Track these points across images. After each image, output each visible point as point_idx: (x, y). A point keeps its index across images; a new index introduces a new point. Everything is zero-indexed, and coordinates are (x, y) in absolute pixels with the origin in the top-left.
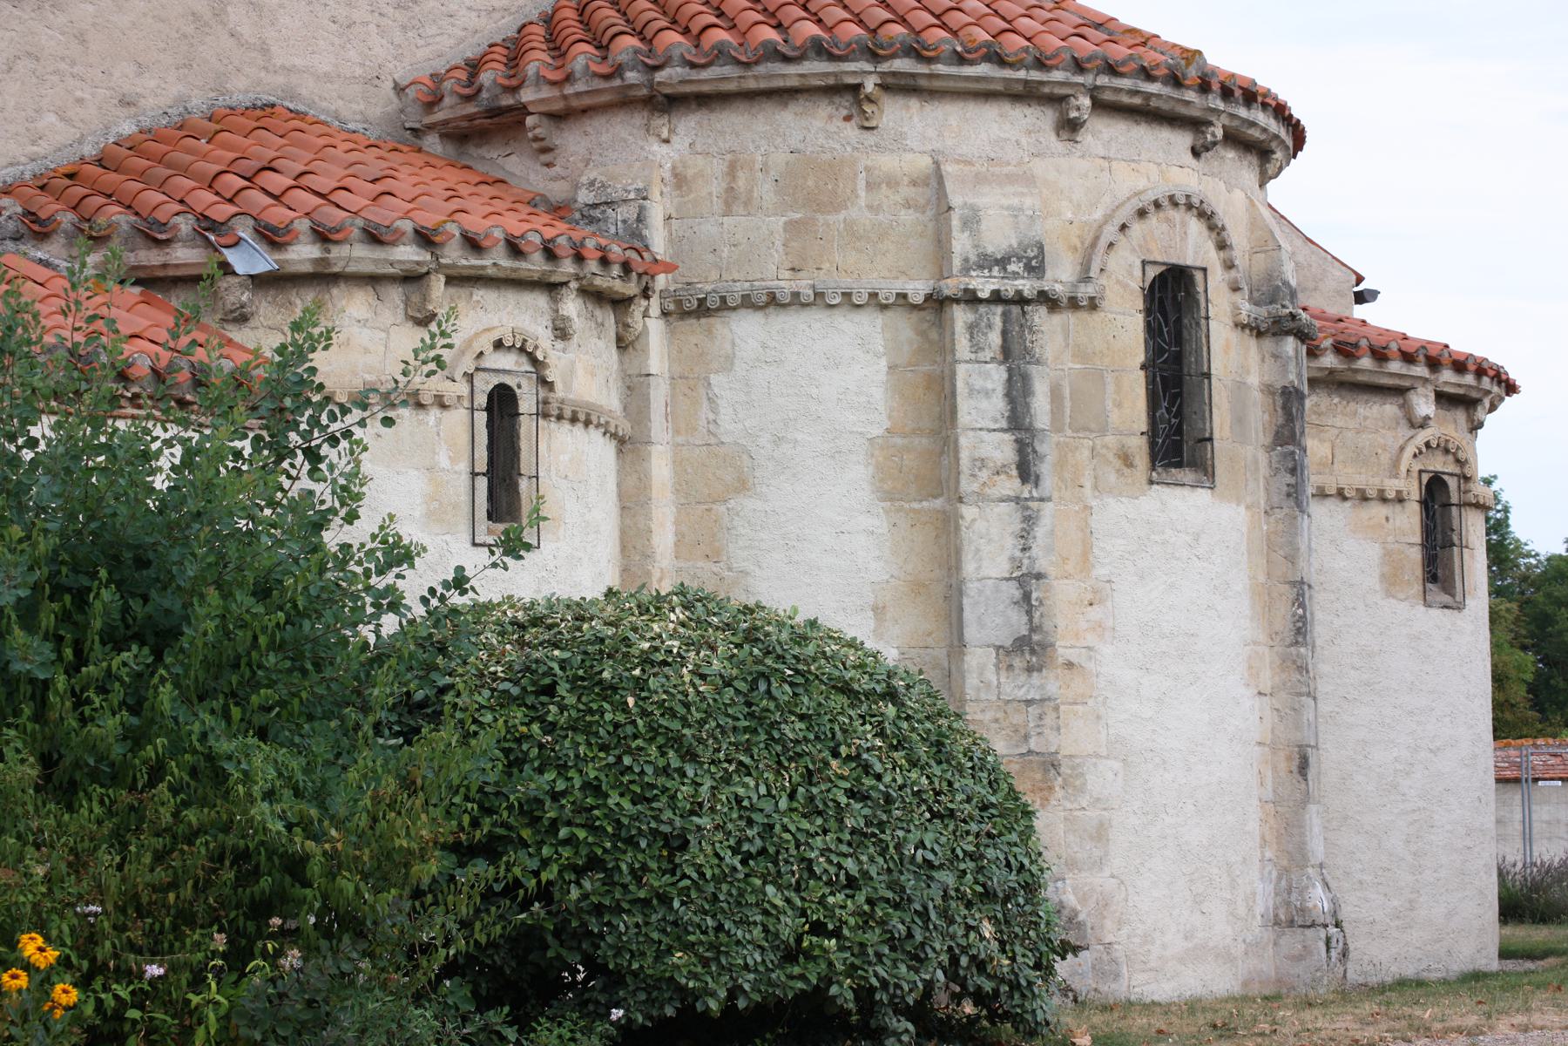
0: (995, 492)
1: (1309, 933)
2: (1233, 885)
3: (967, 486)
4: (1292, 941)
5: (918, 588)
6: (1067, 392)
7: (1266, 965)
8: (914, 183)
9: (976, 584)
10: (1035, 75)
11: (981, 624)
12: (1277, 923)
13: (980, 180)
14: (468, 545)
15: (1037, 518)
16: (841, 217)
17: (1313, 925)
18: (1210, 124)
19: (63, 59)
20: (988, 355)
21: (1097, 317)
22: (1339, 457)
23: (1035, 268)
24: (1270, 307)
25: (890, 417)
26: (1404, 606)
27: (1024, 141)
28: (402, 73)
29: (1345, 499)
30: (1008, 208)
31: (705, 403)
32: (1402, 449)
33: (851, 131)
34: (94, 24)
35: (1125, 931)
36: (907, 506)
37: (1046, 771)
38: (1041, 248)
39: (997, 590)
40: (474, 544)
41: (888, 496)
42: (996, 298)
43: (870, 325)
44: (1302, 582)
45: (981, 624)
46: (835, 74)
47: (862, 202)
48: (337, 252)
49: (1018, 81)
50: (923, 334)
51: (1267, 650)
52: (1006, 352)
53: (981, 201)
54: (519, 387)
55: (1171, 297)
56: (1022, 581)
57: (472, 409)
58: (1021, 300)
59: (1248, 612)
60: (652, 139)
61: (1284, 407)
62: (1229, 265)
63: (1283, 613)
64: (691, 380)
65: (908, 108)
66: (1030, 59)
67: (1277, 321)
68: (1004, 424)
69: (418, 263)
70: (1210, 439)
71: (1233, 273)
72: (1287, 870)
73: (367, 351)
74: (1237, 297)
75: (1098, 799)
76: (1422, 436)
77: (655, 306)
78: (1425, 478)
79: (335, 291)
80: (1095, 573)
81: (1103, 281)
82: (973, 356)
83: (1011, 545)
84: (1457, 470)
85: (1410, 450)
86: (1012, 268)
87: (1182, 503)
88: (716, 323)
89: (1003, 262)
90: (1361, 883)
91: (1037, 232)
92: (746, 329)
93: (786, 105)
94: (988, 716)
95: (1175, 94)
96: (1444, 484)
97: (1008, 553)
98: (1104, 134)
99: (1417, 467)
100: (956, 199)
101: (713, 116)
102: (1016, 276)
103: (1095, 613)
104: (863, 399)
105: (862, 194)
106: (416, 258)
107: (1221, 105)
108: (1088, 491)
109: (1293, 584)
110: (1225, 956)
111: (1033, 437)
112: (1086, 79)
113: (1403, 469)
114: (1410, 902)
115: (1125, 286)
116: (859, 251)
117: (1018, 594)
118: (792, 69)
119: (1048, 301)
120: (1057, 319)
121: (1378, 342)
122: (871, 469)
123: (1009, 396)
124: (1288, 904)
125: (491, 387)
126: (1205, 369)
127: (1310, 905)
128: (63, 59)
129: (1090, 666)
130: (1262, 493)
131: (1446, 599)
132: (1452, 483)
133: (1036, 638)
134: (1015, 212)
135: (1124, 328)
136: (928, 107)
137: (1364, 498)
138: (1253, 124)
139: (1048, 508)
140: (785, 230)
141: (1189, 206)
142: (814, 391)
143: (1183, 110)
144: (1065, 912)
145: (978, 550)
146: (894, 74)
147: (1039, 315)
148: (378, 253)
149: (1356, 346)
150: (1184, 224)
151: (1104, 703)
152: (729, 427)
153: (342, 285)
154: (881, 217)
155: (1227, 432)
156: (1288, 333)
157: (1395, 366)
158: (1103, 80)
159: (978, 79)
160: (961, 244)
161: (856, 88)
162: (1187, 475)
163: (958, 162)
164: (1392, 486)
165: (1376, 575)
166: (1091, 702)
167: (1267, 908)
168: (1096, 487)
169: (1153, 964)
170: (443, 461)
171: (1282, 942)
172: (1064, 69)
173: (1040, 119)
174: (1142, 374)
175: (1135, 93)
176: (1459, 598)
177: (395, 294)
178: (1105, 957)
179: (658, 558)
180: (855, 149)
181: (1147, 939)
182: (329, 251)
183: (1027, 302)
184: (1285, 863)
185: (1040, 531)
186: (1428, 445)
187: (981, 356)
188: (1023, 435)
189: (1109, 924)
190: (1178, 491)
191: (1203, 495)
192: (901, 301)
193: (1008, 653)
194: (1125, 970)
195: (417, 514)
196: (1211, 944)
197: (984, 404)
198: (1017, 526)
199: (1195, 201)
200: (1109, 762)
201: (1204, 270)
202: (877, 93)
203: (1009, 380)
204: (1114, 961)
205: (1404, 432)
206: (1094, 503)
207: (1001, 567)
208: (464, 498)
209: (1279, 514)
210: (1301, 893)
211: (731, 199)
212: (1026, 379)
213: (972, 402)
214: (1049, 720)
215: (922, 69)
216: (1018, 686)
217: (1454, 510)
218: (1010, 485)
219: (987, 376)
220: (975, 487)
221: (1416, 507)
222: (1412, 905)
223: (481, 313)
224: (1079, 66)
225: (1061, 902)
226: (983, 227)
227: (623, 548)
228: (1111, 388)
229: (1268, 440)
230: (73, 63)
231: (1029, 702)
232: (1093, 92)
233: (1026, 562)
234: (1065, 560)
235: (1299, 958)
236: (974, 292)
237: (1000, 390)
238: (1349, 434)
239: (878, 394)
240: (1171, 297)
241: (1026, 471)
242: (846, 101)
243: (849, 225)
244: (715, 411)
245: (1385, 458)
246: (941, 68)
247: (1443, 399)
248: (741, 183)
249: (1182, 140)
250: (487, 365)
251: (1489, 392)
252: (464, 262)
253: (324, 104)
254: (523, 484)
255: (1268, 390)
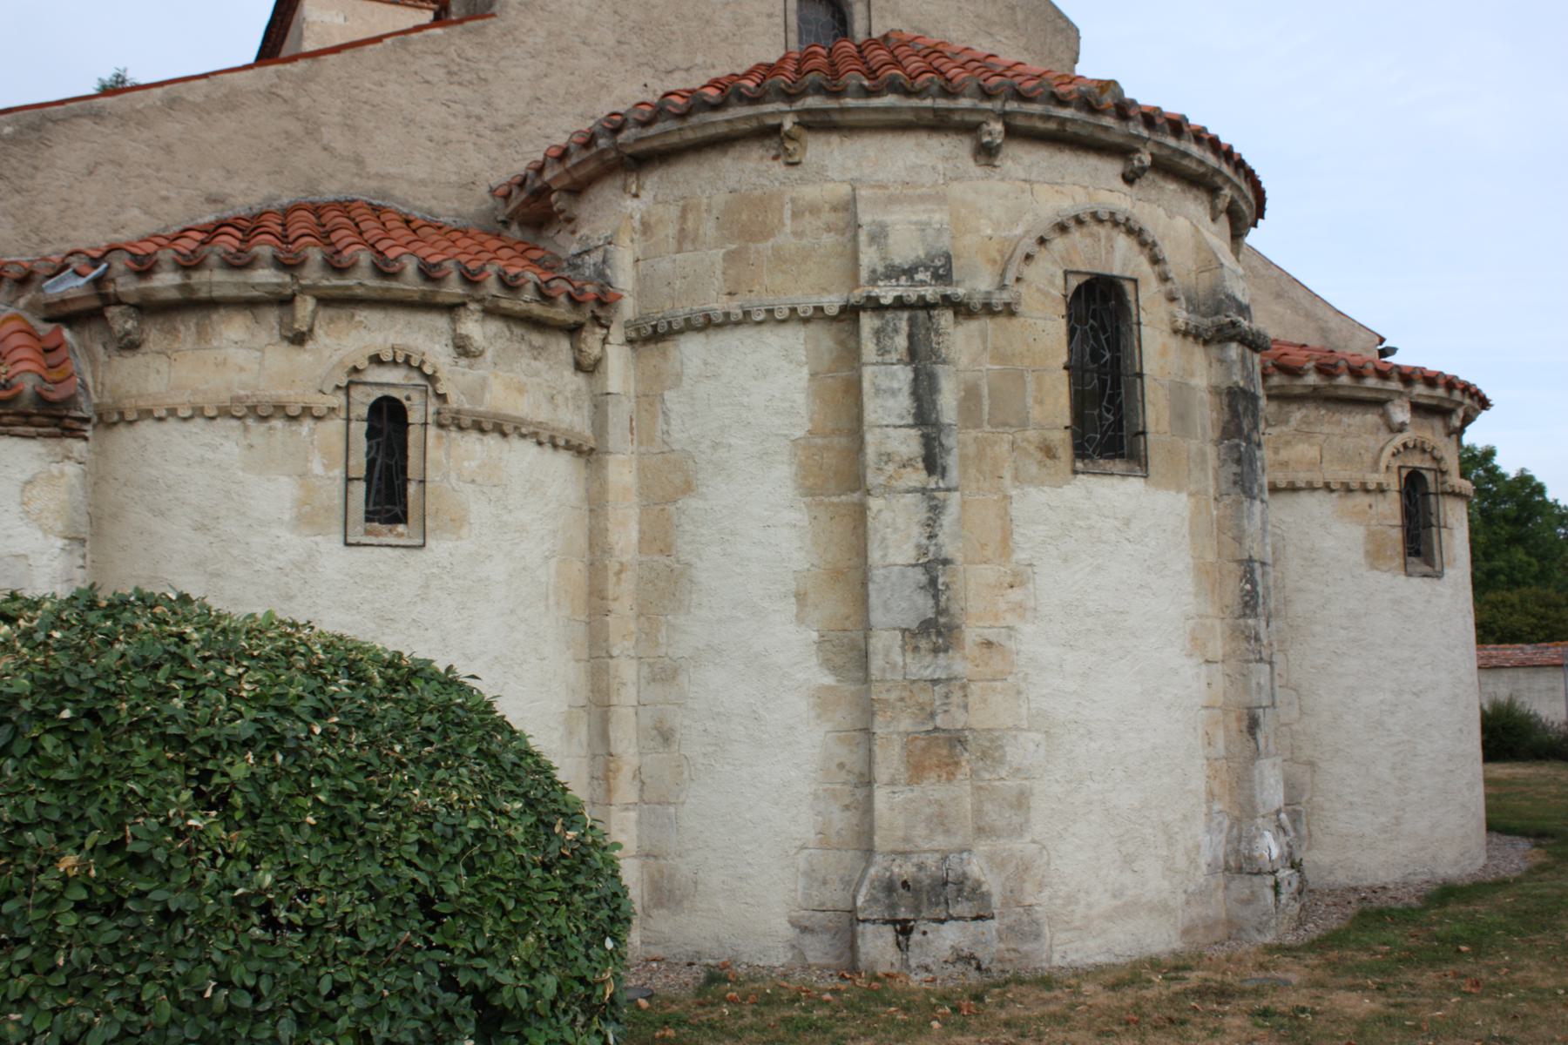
0: (901, 484)
1: (1256, 879)
2: (1170, 840)
3: (872, 479)
4: (1241, 886)
5: (836, 575)
6: (985, 391)
7: (1216, 908)
8: (834, 209)
9: (882, 571)
10: (942, 103)
11: (887, 608)
12: (1227, 868)
13: (892, 200)
14: (341, 545)
15: (944, 507)
16: (770, 243)
17: (1259, 873)
18: (1138, 151)
19: (148, 165)
20: (894, 357)
21: (1015, 323)
22: (1327, 457)
23: (943, 275)
24: (1215, 319)
25: (811, 420)
26: (1387, 576)
27: (940, 167)
28: (494, 182)
29: (1332, 491)
30: (916, 223)
31: (661, 419)
32: (1382, 449)
33: (778, 168)
34: (181, 140)
35: (1047, 892)
36: (826, 500)
37: (952, 747)
38: (948, 258)
39: (903, 575)
40: (347, 544)
41: (810, 492)
42: (900, 304)
43: (795, 339)
44: (1251, 560)
45: (887, 608)
46: (756, 117)
47: (788, 229)
48: (198, 278)
49: (926, 109)
50: (842, 343)
51: (1217, 623)
52: (913, 354)
53: (888, 219)
54: (408, 398)
55: (1099, 308)
56: (928, 567)
57: (348, 420)
58: (925, 305)
59: (1191, 589)
60: (627, 196)
61: (1230, 405)
62: (1164, 278)
63: (1233, 588)
64: (650, 398)
65: (829, 143)
66: (935, 88)
67: (1220, 329)
68: (910, 421)
69: (278, 285)
70: (1144, 433)
71: (1169, 285)
72: (1238, 820)
73: (242, 369)
74: (1174, 307)
75: (1019, 770)
76: (1399, 440)
77: (617, 334)
78: (1404, 473)
79: (215, 317)
80: (1015, 557)
81: (1022, 288)
82: (880, 359)
83: (917, 533)
84: (1434, 466)
85: (1389, 450)
86: (919, 276)
87: (1112, 493)
88: (668, 345)
89: (910, 272)
90: (1351, 803)
91: (945, 243)
92: (691, 350)
93: (726, 152)
94: (894, 696)
95: (1091, 119)
96: (1423, 477)
97: (914, 541)
98: (1022, 160)
99: (1395, 464)
100: (865, 218)
101: (671, 170)
102: (923, 283)
103: (1015, 595)
104: (787, 405)
105: (788, 222)
106: (275, 280)
107: (1145, 133)
108: (1007, 481)
109: (1240, 562)
110: (1163, 909)
111: (940, 431)
112: (996, 105)
113: (1383, 465)
114: (1396, 818)
115: (1046, 294)
116: (783, 272)
117: (924, 579)
118: (719, 116)
119: (962, 309)
120: (973, 326)
121: (1355, 362)
122: (794, 467)
123: (916, 394)
124: (1237, 852)
125: (372, 399)
126: (1137, 369)
127: (1257, 854)
128: (148, 165)
129: (1012, 645)
130: (1211, 482)
131: (1427, 569)
132: (1430, 477)
133: (942, 620)
134: (922, 227)
135: (1046, 332)
136: (847, 142)
137: (1348, 489)
138: (1186, 155)
139: (955, 497)
140: (724, 260)
141: (1116, 224)
142: (745, 400)
143: (1103, 136)
144: (969, 883)
145: (884, 539)
146: (809, 111)
147: (945, 318)
148: (238, 277)
149: (1335, 366)
150: (1109, 239)
151: (1025, 679)
152: (680, 435)
153: (222, 312)
154: (804, 242)
155: (1164, 425)
156: (1231, 339)
157: (1371, 382)
158: (1012, 106)
159: (887, 110)
160: (869, 257)
161: (777, 129)
162: (1119, 466)
163: (873, 187)
164: (1373, 479)
165: (1362, 551)
166: (1010, 679)
167: (1216, 858)
168: (1016, 478)
169: (1077, 924)
170: (317, 467)
171: (1232, 886)
172: (971, 96)
173: (960, 147)
174: (1065, 373)
175: (1048, 118)
176: (1438, 568)
177: (272, 316)
178: (1025, 919)
179: (617, 553)
180: (782, 183)
181: (1071, 900)
182: (189, 277)
183: (933, 306)
184: (1237, 813)
185: (947, 520)
186: (1405, 445)
187: (887, 358)
188: (929, 430)
189: (1028, 887)
190: (1107, 480)
191: (1135, 485)
192: (820, 314)
193: (914, 635)
194: (1046, 930)
195: (287, 517)
196: (1143, 900)
197: (891, 403)
198: (923, 515)
199: (1121, 218)
200: (1032, 735)
201: (1135, 281)
202: (797, 131)
203: (916, 380)
204: (1035, 922)
205: (1384, 435)
206: (1014, 493)
207: (907, 554)
208: (338, 501)
209: (1227, 500)
210: (1249, 843)
211: (684, 238)
212: (932, 378)
213: (878, 401)
214: (956, 698)
215: (832, 104)
216: (923, 666)
217: (1432, 499)
218: (917, 477)
219: (893, 376)
220: (882, 479)
221: (1396, 496)
222: (1398, 821)
223: (363, 332)
224: (987, 94)
225: (964, 874)
226: (890, 241)
227: (591, 546)
228: (1031, 386)
229: (1216, 435)
230: (158, 170)
231: (935, 682)
232: (1004, 116)
233: (932, 549)
234: (984, 546)
235: (1247, 902)
236: (877, 299)
237: (906, 389)
238: (1335, 439)
239: (800, 399)
240: (1099, 308)
241: (932, 463)
242: (772, 143)
243: (776, 250)
244: (667, 423)
245: (1368, 458)
246: (849, 102)
247: (1417, 408)
248: (690, 224)
249: (1111, 169)
250: (370, 379)
251: (1460, 404)
252: (326, 283)
253: (418, 203)
254: (412, 488)
255: (1215, 390)
